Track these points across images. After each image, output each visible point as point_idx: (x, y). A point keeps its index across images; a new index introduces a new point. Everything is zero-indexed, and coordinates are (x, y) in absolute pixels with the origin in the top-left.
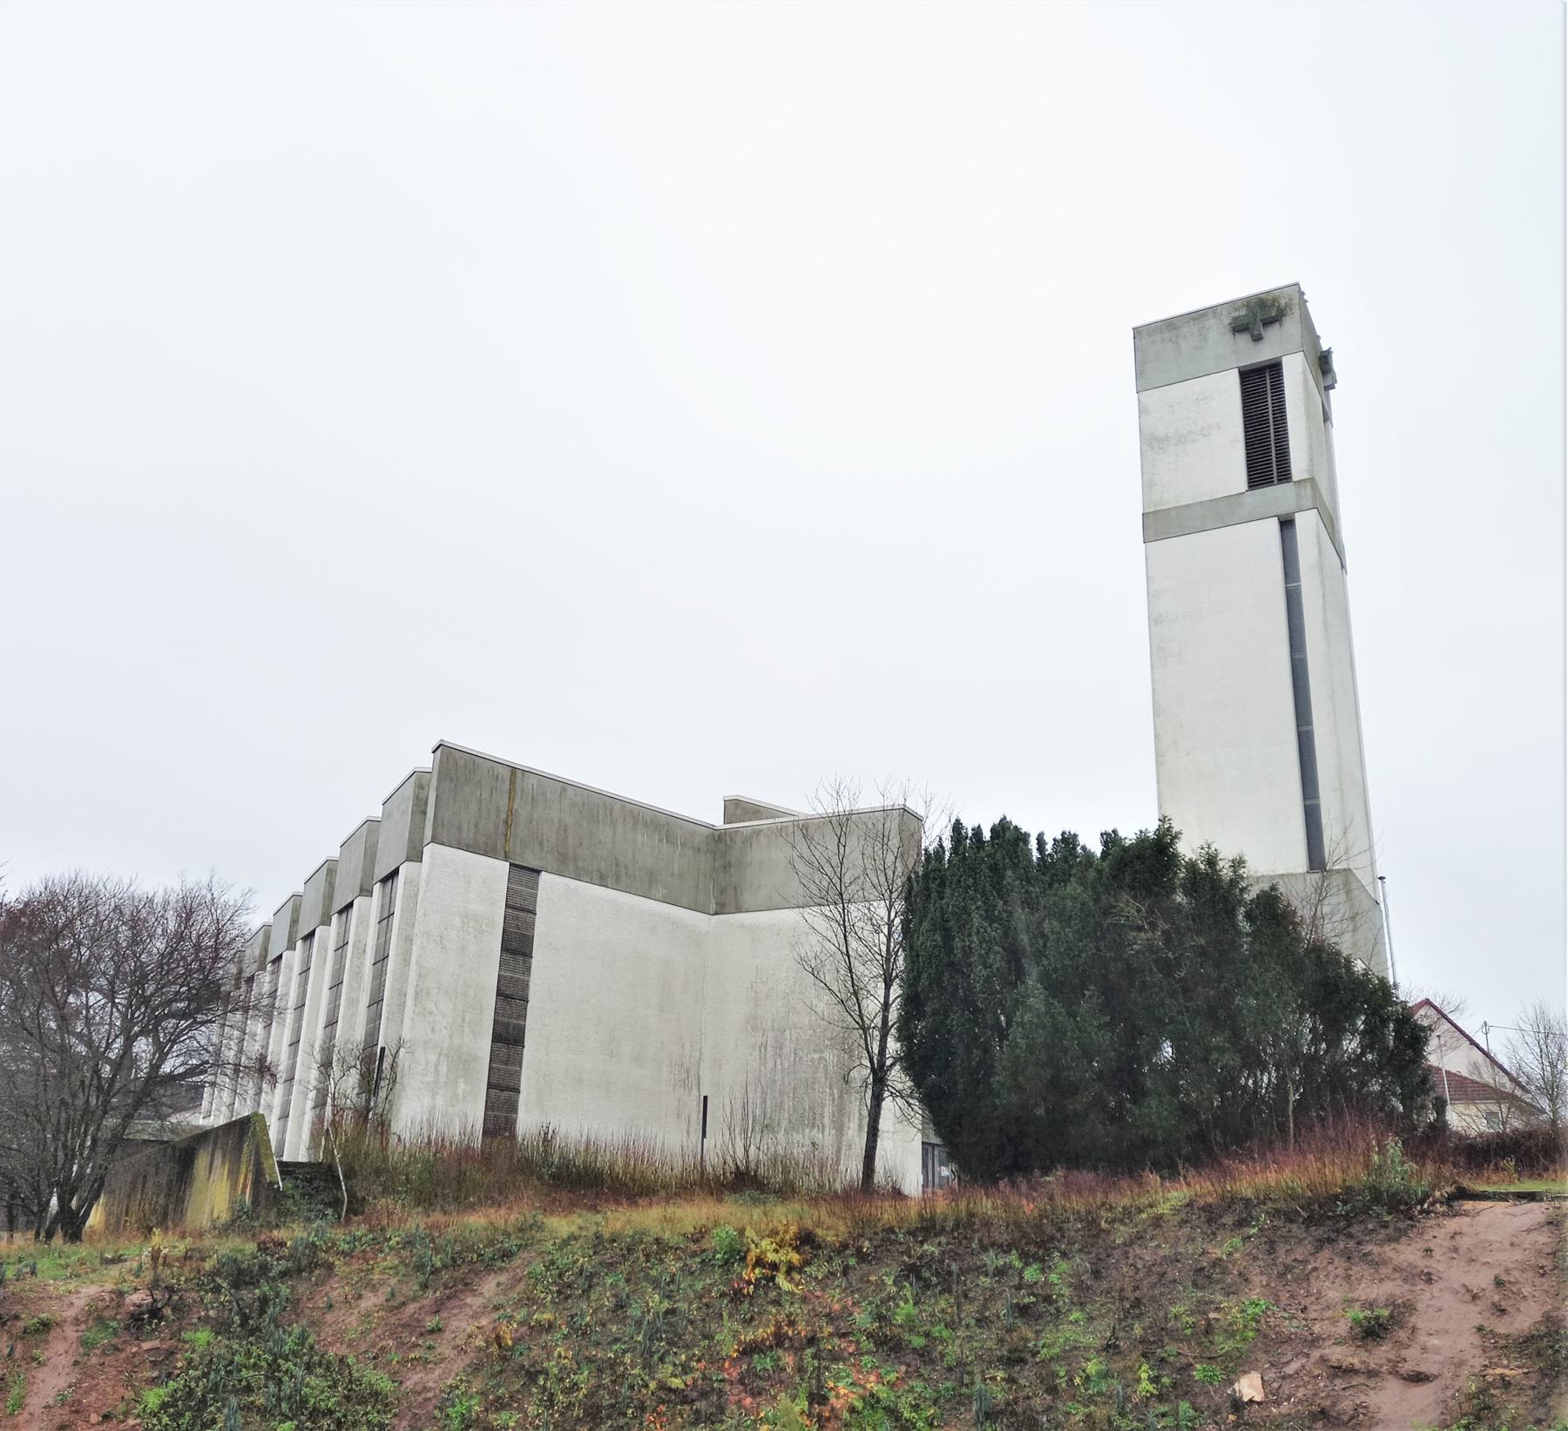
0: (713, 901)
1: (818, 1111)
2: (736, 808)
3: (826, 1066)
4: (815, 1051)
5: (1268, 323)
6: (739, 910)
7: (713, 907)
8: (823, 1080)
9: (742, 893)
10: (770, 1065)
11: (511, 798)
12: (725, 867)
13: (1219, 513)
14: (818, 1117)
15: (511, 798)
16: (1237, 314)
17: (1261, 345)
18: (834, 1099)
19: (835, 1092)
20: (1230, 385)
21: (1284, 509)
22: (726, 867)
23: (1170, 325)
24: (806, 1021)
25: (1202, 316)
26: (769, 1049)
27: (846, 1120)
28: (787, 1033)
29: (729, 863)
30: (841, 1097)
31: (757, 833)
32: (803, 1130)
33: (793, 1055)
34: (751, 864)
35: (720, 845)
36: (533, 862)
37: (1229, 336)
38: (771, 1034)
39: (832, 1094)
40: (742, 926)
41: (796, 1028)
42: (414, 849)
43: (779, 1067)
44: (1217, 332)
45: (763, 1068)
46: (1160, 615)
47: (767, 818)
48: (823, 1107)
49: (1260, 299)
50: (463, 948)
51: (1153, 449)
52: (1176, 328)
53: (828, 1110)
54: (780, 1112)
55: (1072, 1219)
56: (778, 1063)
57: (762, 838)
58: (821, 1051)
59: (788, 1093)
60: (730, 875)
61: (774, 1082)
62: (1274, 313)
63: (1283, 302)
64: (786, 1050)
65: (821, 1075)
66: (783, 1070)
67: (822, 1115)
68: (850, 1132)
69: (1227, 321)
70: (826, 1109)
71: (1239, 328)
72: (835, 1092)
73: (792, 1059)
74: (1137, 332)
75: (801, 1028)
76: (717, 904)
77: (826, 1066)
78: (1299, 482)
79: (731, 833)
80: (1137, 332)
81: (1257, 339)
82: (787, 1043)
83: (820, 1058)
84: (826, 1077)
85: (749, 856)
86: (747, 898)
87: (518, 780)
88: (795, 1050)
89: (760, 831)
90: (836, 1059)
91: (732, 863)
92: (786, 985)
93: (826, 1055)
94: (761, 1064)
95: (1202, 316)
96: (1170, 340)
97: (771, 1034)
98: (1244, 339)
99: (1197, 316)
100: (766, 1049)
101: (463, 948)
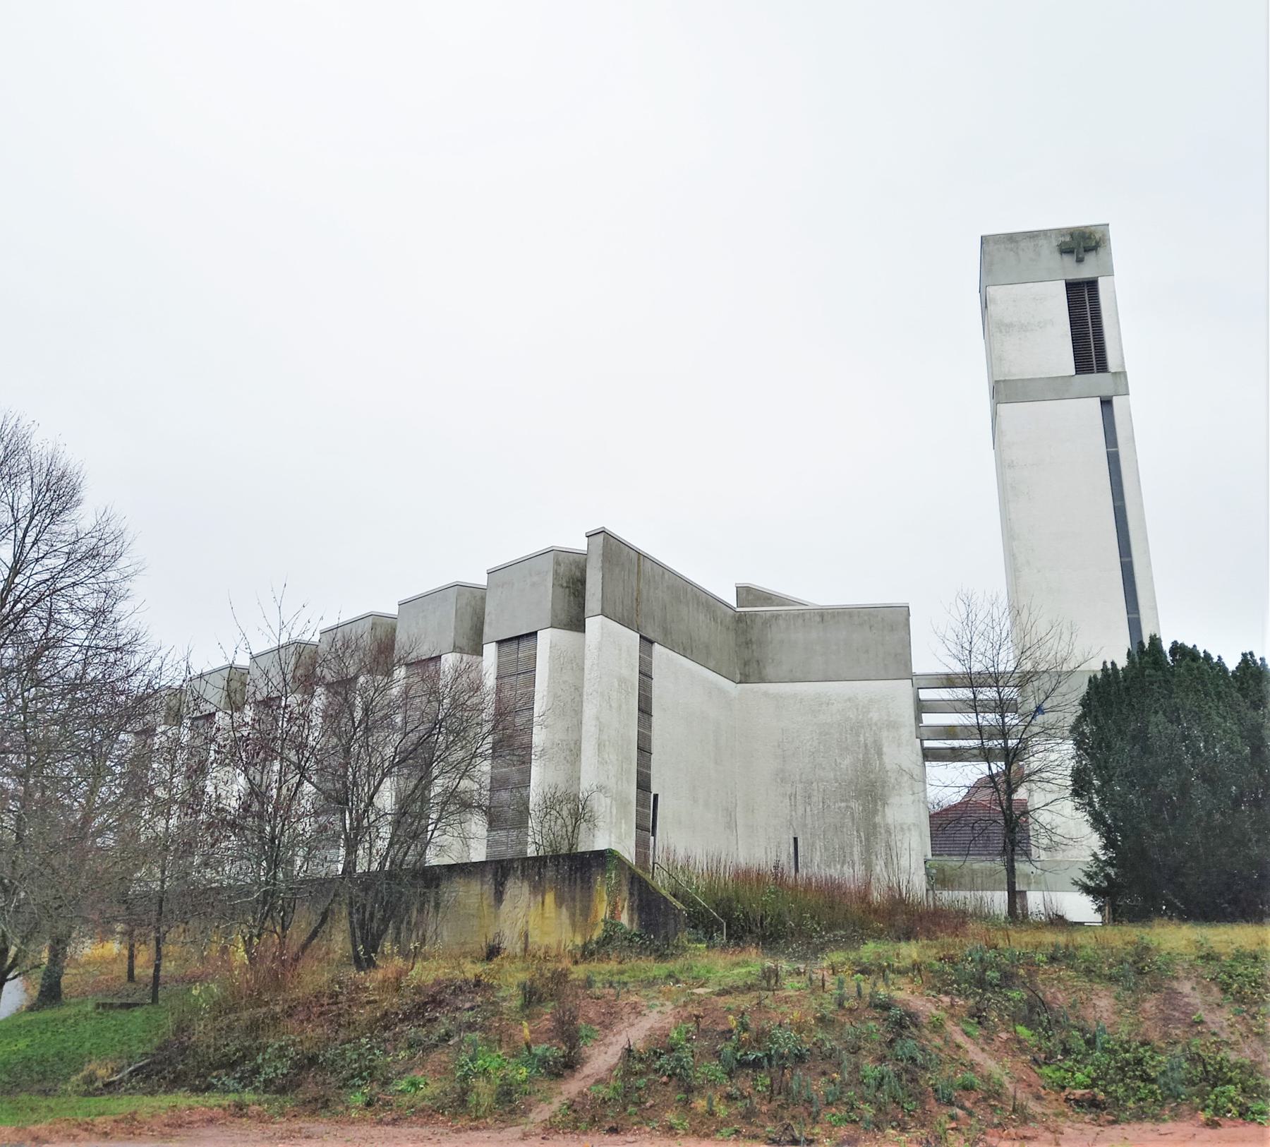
0: (738, 672)
1: (847, 850)
2: (747, 594)
3: (852, 814)
4: (842, 801)
5: (1087, 250)
6: (762, 680)
7: (738, 677)
8: (850, 824)
9: (764, 667)
10: (800, 811)
11: (639, 580)
12: (747, 644)
13: (1051, 389)
14: (848, 855)
15: (639, 580)
16: (1063, 239)
17: (1081, 266)
18: (861, 841)
19: (862, 834)
20: (1058, 293)
21: (1106, 392)
22: (748, 643)
23: (1011, 238)
24: (832, 775)
25: (1037, 236)
26: (798, 797)
27: (874, 858)
28: (814, 784)
29: (751, 640)
30: (867, 839)
31: (776, 617)
32: (835, 865)
33: (821, 804)
34: (771, 642)
35: (741, 625)
36: (651, 636)
37: (1057, 255)
38: (800, 786)
39: (859, 837)
40: (766, 694)
41: (823, 781)
42: (556, 617)
43: (809, 812)
44: (1048, 250)
45: (793, 813)
46: (1012, 462)
47: (778, 606)
48: (852, 847)
49: (1084, 233)
50: (620, 706)
51: (1001, 331)
52: (1017, 242)
53: (857, 850)
54: (812, 850)
55: (23, 947)
56: (808, 809)
57: (781, 622)
58: (847, 801)
59: (819, 836)
60: (753, 652)
61: (805, 825)
62: (1094, 244)
63: (1097, 236)
64: (814, 799)
65: (848, 821)
66: (812, 815)
67: (851, 854)
68: (878, 868)
69: (1055, 243)
70: (855, 849)
71: (1065, 250)
72: (862, 834)
73: (821, 807)
74: (984, 240)
75: (827, 782)
76: (741, 674)
77: (852, 814)
78: (1116, 373)
79: (752, 615)
80: (984, 240)
81: (1080, 260)
82: (815, 793)
83: (847, 807)
84: (853, 824)
85: (769, 636)
86: (769, 671)
87: (642, 563)
88: (823, 799)
89: (779, 615)
90: (861, 808)
91: (753, 640)
92: (811, 745)
93: (852, 805)
94: (791, 811)
95: (1037, 236)
96: (1011, 250)
97: (800, 786)
98: (1069, 260)
99: (1032, 235)
100: (795, 798)
101: (620, 706)
